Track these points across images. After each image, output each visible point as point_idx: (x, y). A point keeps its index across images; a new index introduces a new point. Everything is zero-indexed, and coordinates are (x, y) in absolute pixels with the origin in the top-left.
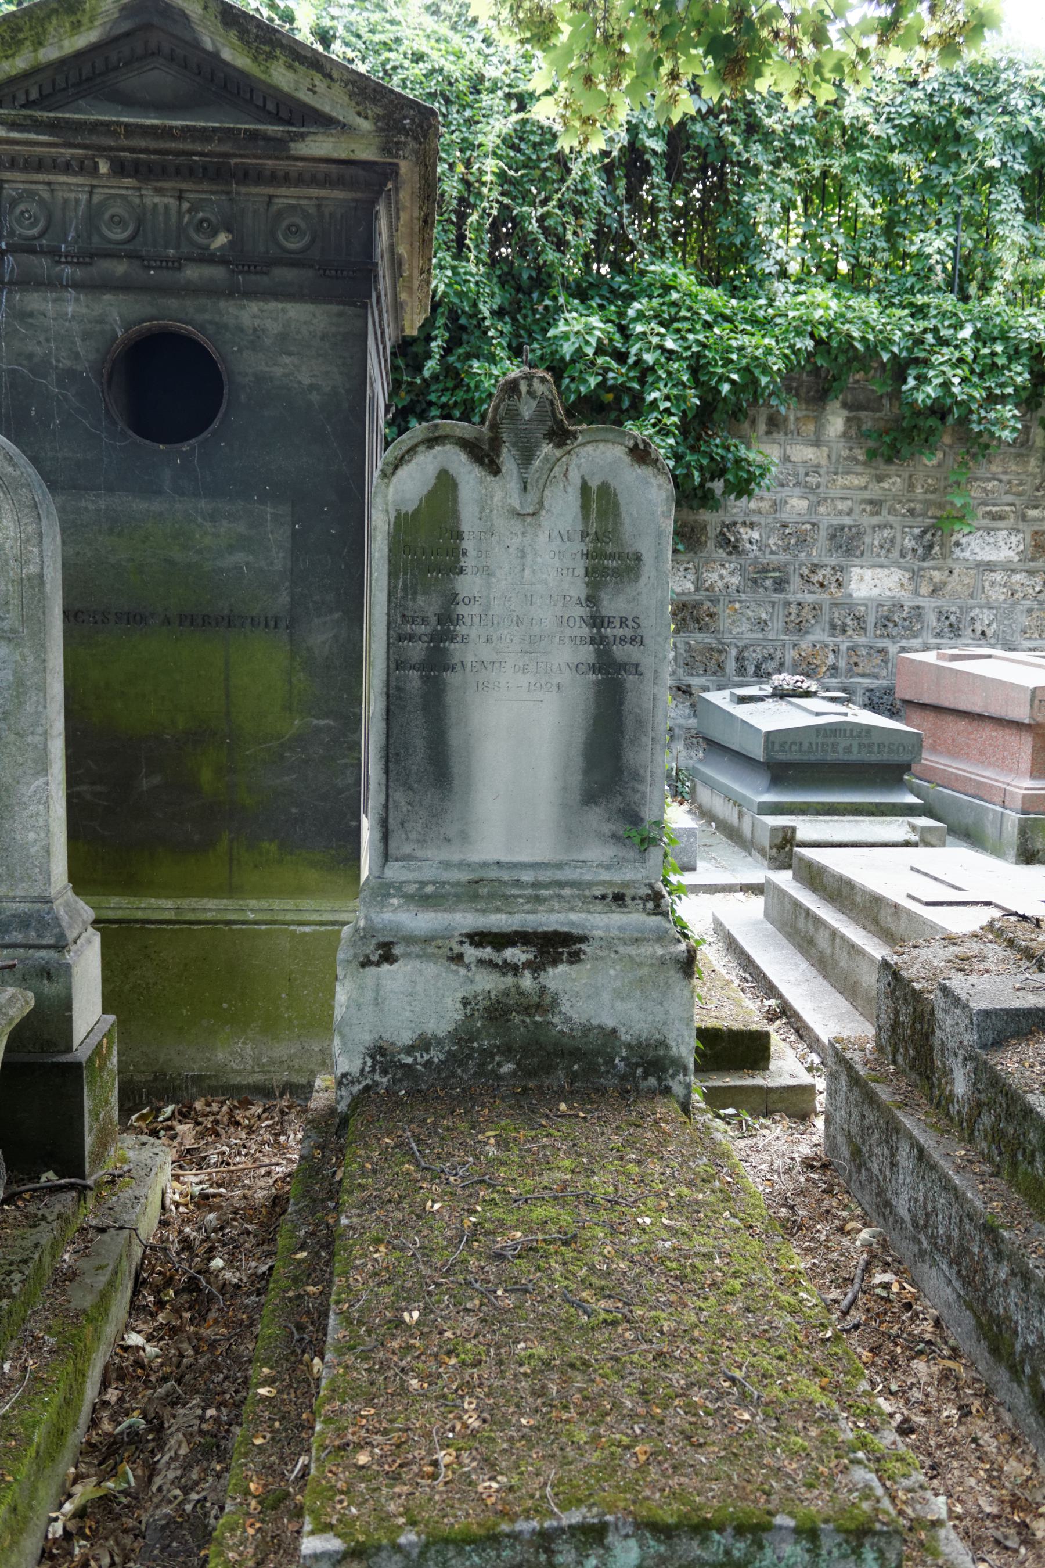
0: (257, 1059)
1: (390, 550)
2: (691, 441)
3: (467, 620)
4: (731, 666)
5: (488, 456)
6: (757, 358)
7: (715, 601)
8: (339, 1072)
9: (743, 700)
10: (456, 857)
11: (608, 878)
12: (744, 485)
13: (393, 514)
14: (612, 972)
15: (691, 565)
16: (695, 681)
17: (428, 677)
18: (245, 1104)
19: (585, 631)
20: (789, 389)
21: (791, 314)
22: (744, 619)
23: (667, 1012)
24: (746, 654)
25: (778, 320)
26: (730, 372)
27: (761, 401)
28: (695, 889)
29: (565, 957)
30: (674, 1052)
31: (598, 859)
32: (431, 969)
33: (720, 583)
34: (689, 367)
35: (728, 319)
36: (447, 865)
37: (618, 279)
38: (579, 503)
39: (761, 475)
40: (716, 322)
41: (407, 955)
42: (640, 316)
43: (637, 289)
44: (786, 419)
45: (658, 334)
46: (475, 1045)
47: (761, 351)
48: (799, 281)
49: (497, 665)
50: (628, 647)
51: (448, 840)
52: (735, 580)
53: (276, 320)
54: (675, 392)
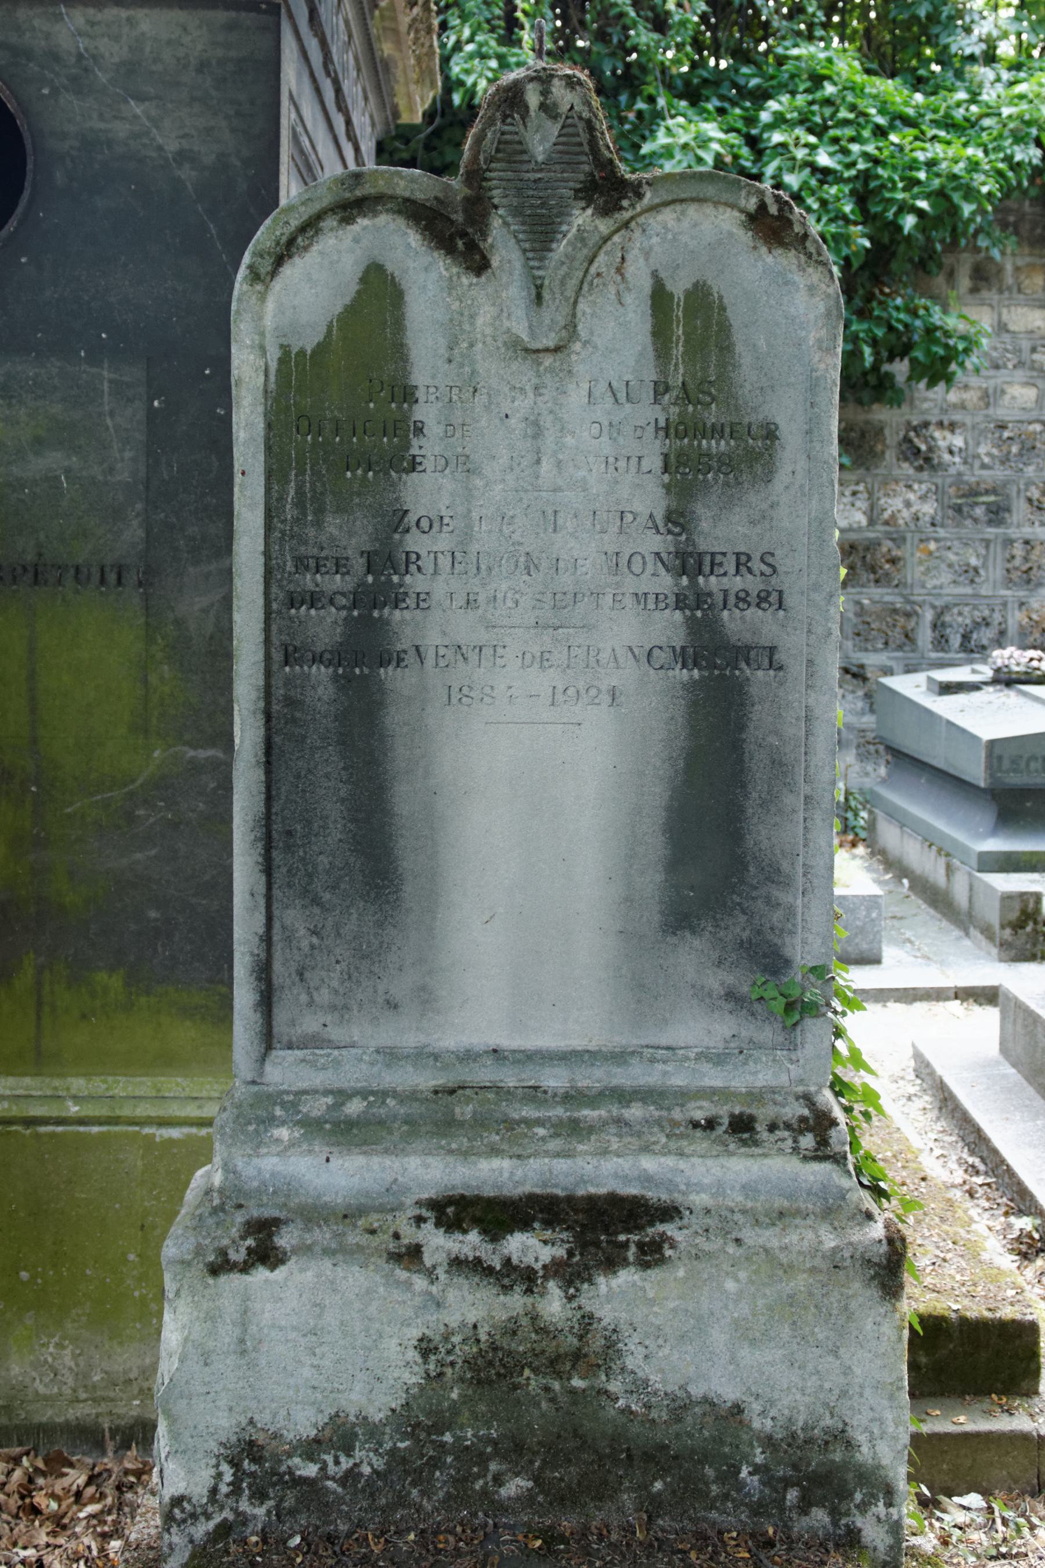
0: (82, 1376)
1: (269, 426)
2: (858, 302)
3: (427, 563)
4: (925, 636)
5: (463, 235)
6: (955, 177)
7: (899, 540)
8: (169, 1492)
9: (948, 689)
10: (410, 1040)
11: (718, 1083)
12: (938, 365)
13: (274, 354)
14: (730, 1285)
15: (861, 487)
16: (872, 660)
17: (349, 678)
18: (56, 1464)
19: (665, 583)
20: (1004, 225)
21: (1006, 111)
22: (943, 566)
23: (847, 1371)
24: (947, 618)
25: (987, 122)
26: (915, 197)
27: (963, 242)
28: (882, 996)
29: (632, 1253)
30: (864, 1454)
31: (699, 1044)
32: (354, 1278)
33: (906, 514)
34: (853, 192)
35: (908, 122)
36: (391, 1056)
37: (745, 70)
38: (648, 327)
39: (966, 351)
40: (892, 127)
41: (305, 1250)
42: (779, 121)
43: (774, 83)
44: (1000, 270)
45: (806, 145)
46: (448, 1438)
47: (962, 165)
48: (1017, 67)
49: (487, 652)
50: (752, 613)
51: (392, 1006)
52: (928, 509)
53: (117, 38)
54: (832, 228)
